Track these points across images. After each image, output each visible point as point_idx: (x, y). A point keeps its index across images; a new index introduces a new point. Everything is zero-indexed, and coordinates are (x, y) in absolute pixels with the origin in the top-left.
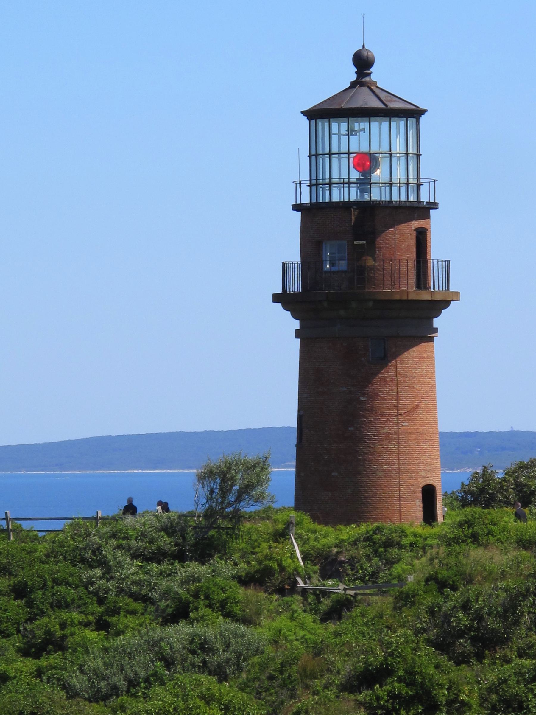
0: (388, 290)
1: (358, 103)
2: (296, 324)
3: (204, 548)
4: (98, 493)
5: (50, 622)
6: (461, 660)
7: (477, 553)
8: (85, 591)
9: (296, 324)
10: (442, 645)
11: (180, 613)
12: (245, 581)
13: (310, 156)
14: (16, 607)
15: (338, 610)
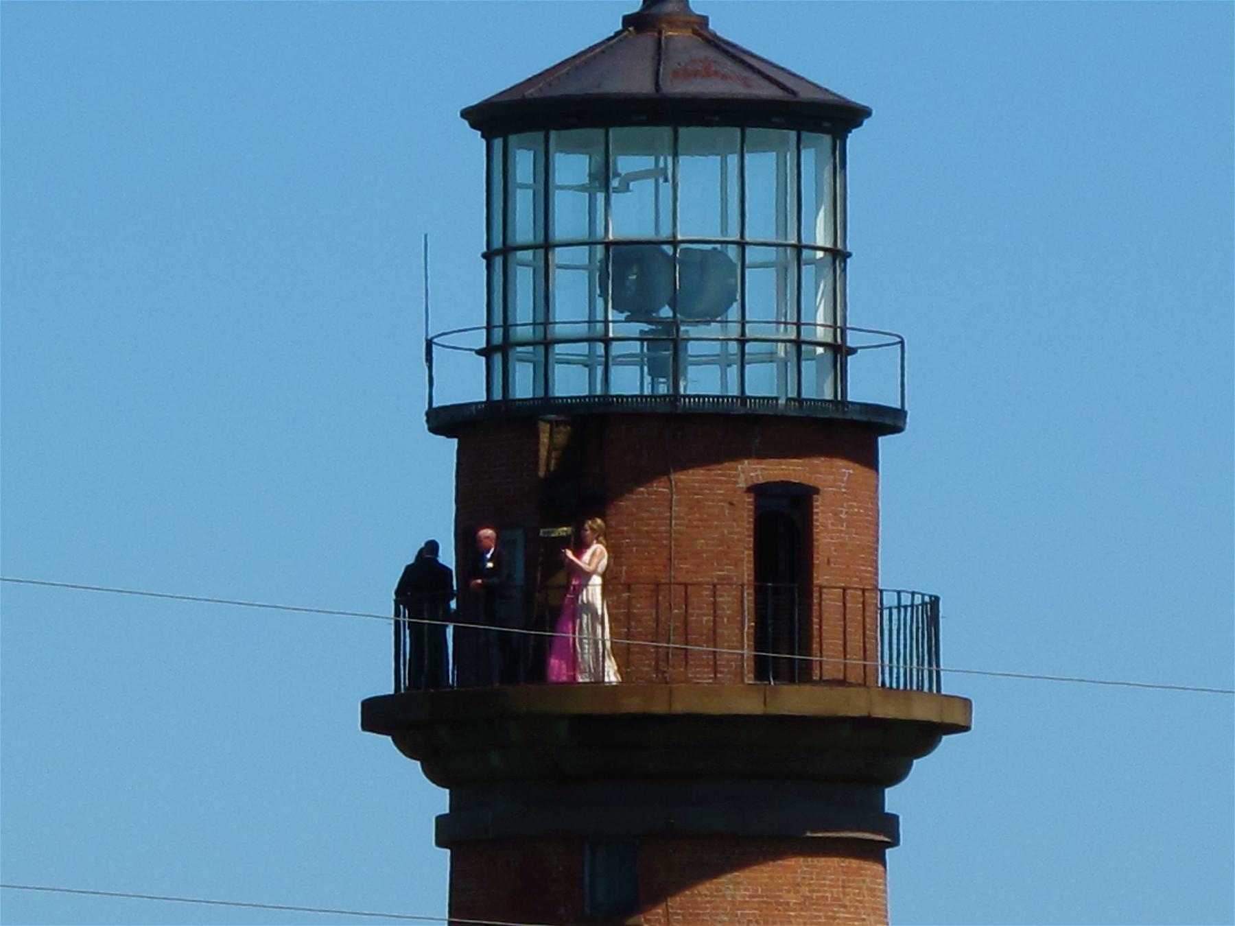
2: (440, 800)
9: (440, 800)
13: (488, 256)
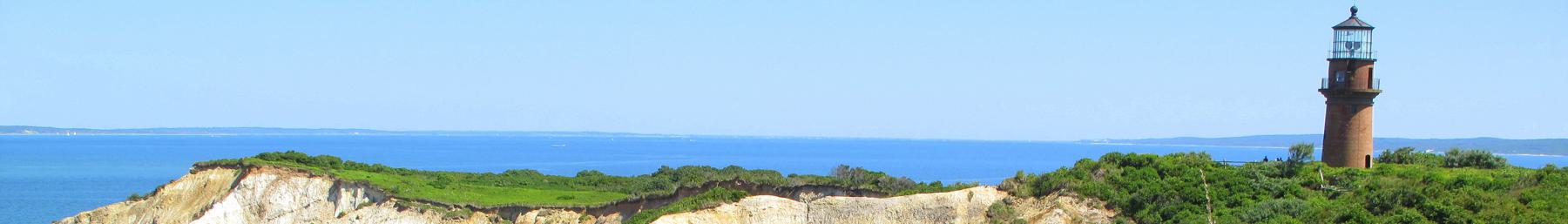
0: (1357, 88)
1: (1351, 24)
3: (1290, 174)
4: (1254, 155)
5: (1237, 196)
6: (1376, 214)
7: (1383, 178)
8: (1438, 204)
10: (1370, 209)
11: (1281, 195)
12: (1303, 185)
14: (1226, 191)
15: (1335, 196)
